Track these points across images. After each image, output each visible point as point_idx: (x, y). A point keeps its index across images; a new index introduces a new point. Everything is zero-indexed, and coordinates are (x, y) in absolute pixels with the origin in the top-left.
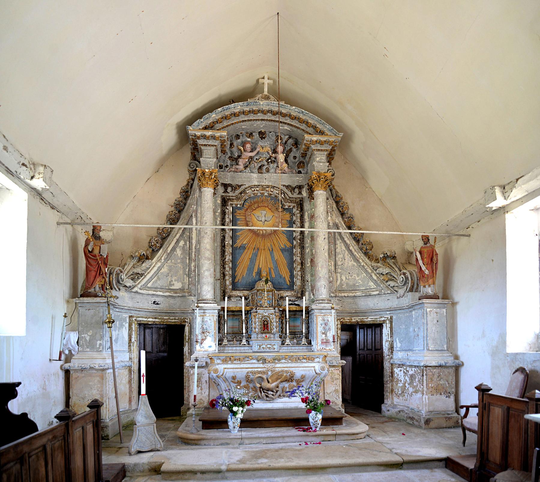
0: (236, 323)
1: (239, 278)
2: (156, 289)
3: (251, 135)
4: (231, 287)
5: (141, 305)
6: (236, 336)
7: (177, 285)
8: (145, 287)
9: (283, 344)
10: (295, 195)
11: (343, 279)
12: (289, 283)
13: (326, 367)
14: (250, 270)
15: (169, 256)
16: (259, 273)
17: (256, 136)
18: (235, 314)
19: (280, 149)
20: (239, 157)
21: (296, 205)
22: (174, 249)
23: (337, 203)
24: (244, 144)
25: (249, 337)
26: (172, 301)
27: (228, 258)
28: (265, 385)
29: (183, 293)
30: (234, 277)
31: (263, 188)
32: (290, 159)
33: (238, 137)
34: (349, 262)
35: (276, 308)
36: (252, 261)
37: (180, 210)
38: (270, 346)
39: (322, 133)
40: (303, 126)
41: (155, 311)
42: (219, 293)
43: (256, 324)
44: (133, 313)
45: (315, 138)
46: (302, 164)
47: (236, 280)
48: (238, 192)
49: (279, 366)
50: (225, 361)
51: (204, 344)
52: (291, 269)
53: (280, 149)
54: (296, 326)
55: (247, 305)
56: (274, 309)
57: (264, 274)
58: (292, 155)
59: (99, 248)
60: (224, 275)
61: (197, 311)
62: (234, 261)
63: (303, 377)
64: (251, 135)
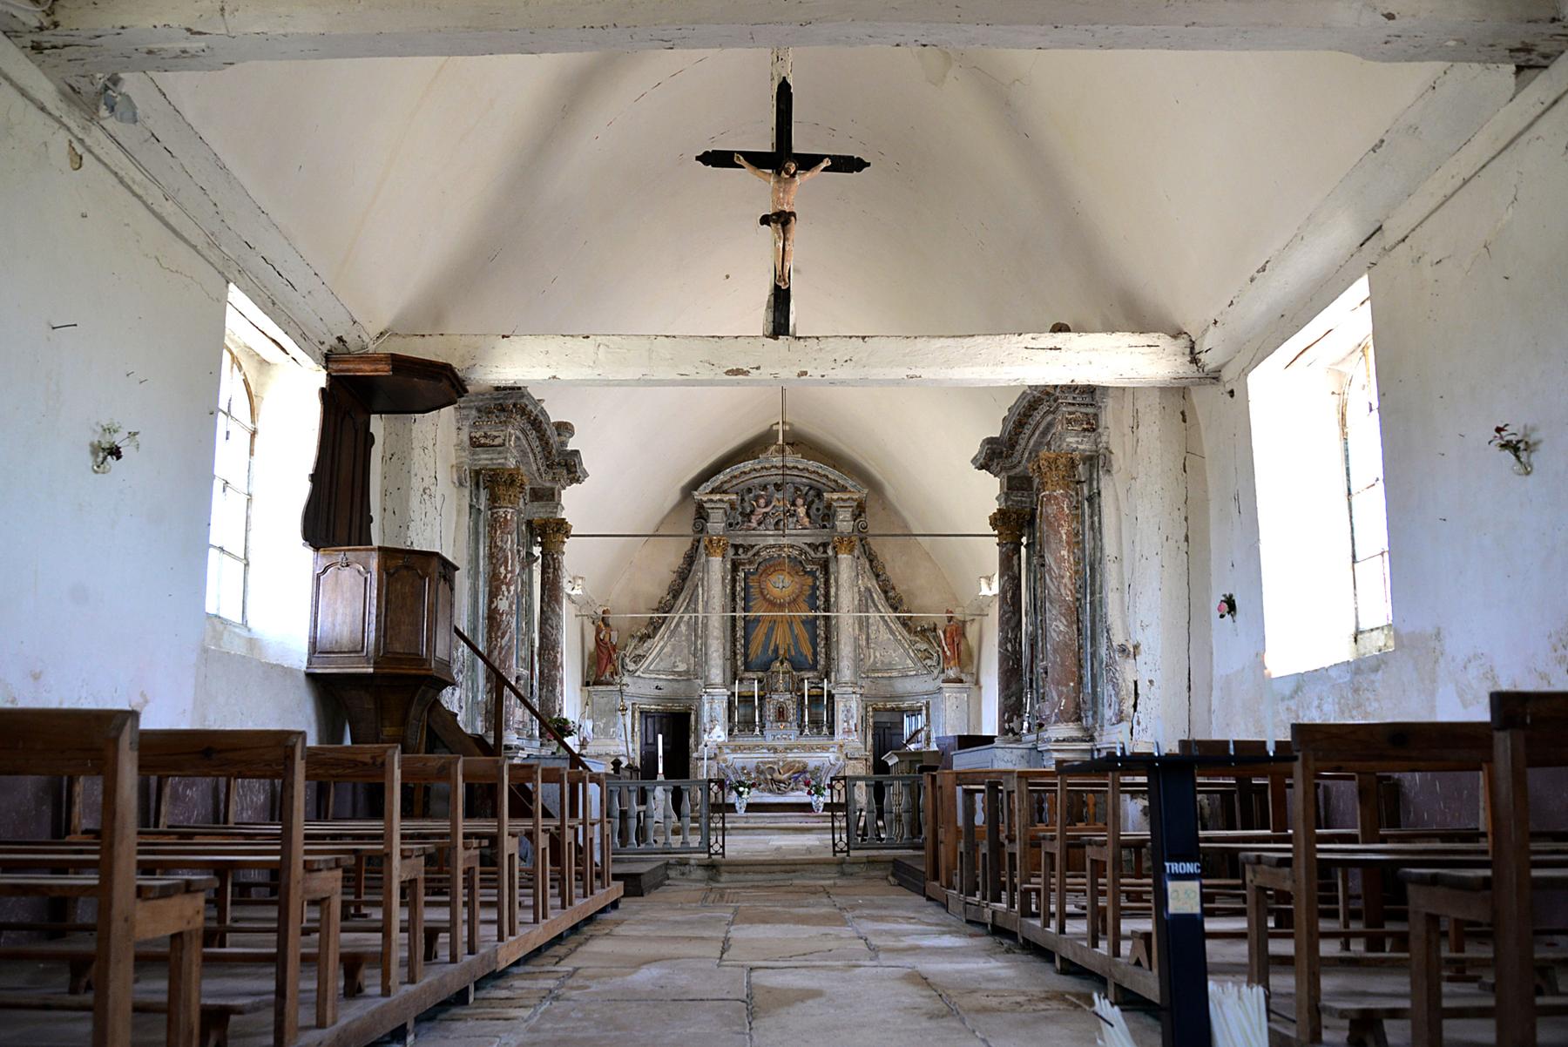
0: (749, 710)
1: (752, 656)
2: (658, 672)
3: (765, 488)
5: (642, 691)
6: (748, 725)
7: (682, 667)
8: (647, 670)
10: (819, 555)
11: (875, 655)
13: (842, 757)
14: (766, 647)
15: (673, 633)
16: (776, 650)
17: (771, 488)
18: (747, 699)
19: (800, 501)
20: (752, 512)
21: (816, 569)
22: (678, 625)
23: (871, 561)
24: (757, 498)
25: (763, 727)
26: (676, 685)
27: (740, 633)
28: (777, 776)
29: (688, 676)
30: (746, 655)
31: (781, 547)
32: (813, 511)
33: (749, 490)
34: (885, 635)
36: (768, 636)
37: (683, 580)
39: (844, 489)
40: (824, 480)
41: (658, 698)
42: (729, 674)
43: (770, 711)
44: (636, 700)
45: (835, 496)
46: (826, 517)
48: (750, 553)
49: (791, 756)
50: (734, 751)
51: (715, 734)
52: (815, 645)
53: (800, 501)
54: (818, 714)
55: (760, 689)
57: (781, 652)
58: (814, 506)
59: (1293, 1017)
60: (735, 654)
61: (705, 697)
62: (746, 637)
63: (817, 769)
64: (765, 488)
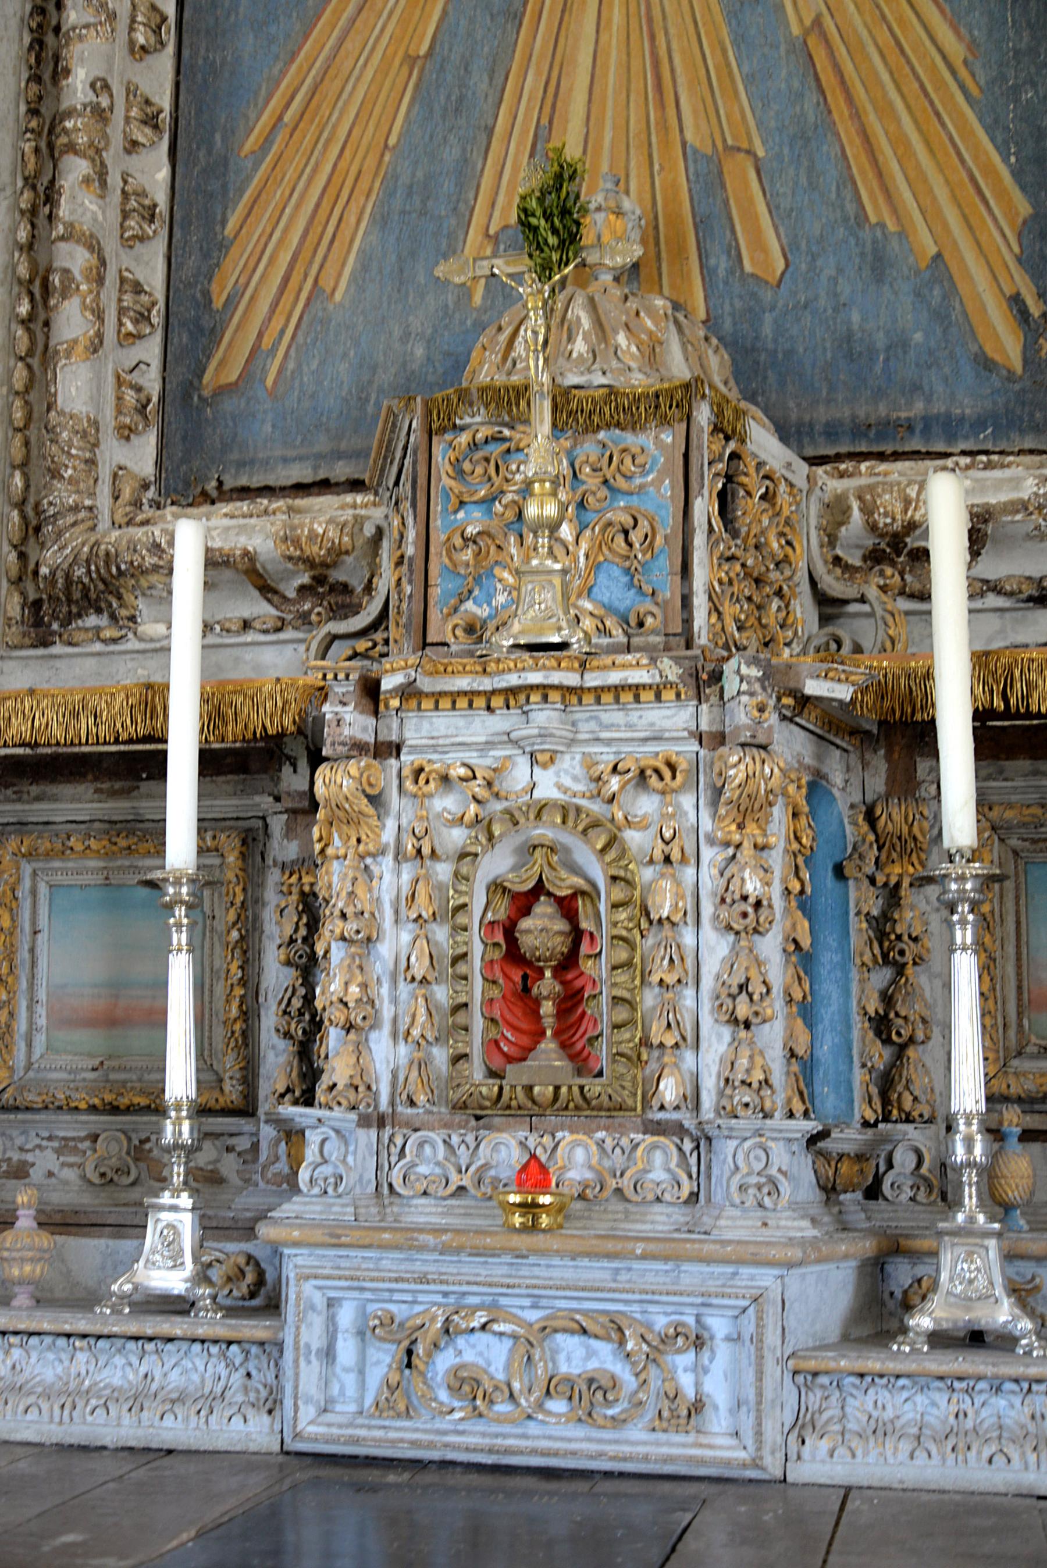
4: (141, 456)
9: (880, 1311)
12: (1008, 345)
30: (191, 324)
35: (739, 674)
38: (603, 1358)
47: (225, 367)
56: (704, 681)
